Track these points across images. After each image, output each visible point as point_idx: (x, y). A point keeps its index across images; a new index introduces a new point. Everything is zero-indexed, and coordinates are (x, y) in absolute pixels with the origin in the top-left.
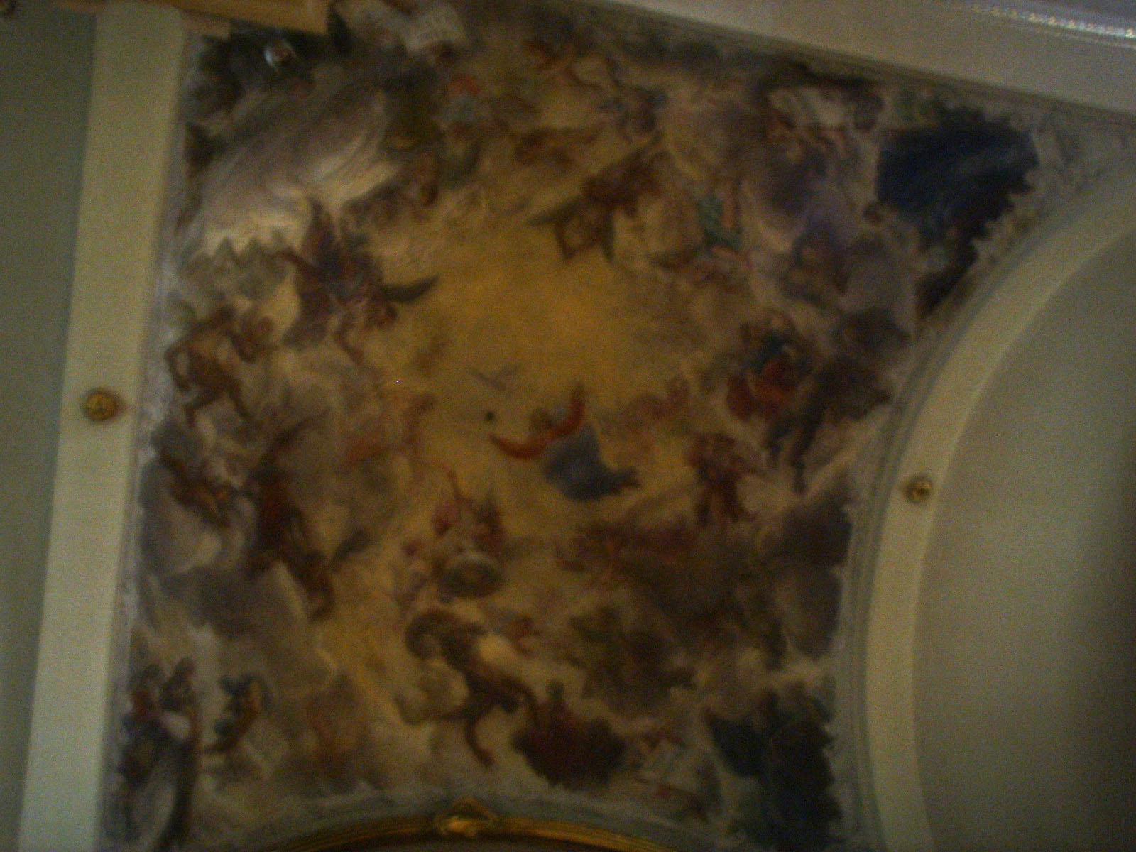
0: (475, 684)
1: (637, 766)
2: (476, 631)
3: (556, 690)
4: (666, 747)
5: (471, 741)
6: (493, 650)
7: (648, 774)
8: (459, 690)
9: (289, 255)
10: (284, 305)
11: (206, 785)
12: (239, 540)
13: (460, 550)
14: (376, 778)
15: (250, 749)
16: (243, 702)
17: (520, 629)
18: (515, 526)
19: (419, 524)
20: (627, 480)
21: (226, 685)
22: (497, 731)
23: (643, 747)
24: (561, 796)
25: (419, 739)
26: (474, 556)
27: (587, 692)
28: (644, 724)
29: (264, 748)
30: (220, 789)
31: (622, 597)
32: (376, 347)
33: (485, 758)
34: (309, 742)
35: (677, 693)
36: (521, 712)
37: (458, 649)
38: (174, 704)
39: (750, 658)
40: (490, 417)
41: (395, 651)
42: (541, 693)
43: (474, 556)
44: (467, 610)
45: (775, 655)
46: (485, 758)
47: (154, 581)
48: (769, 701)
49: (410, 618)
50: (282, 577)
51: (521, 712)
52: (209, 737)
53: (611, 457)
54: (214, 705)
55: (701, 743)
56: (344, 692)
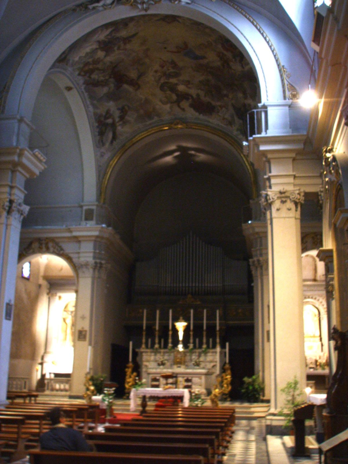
0: (177, 95)
1: (218, 112)
2: (177, 84)
3: (198, 95)
4: (224, 109)
5: (179, 106)
6: (181, 88)
7: (220, 114)
8: (174, 97)
9: (96, 49)
10: (101, 54)
11: (119, 128)
12: (112, 85)
13: (168, 70)
14: (159, 115)
15: (127, 118)
16: (123, 111)
17: (187, 83)
18: (181, 64)
19: (157, 67)
20: (203, 58)
21: (119, 109)
22: (185, 104)
23: (219, 108)
24: (201, 116)
25: (167, 107)
26: (172, 70)
27: (205, 96)
28: (219, 104)
29: (131, 117)
30: (122, 128)
31: (210, 78)
32: (128, 46)
33: (183, 110)
34: (142, 112)
35: (225, 98)
36: (190, 100)
37: (173, 89)
38: (106, 118)
39: (240, 95)
40: (165, 48)
41: (158, 91)
42: (195, 96)
43: (172, 70)
44: (174, 81)
45: (246, 98)
46: (183, 110)
47: (95, 102)
49: (160, 84)
50: (125, 86)
51: (190, 100)
52: (117, 120)
53: (198, 53)
54: (117, 114)
55: (232, 110)
56: (147, 101)
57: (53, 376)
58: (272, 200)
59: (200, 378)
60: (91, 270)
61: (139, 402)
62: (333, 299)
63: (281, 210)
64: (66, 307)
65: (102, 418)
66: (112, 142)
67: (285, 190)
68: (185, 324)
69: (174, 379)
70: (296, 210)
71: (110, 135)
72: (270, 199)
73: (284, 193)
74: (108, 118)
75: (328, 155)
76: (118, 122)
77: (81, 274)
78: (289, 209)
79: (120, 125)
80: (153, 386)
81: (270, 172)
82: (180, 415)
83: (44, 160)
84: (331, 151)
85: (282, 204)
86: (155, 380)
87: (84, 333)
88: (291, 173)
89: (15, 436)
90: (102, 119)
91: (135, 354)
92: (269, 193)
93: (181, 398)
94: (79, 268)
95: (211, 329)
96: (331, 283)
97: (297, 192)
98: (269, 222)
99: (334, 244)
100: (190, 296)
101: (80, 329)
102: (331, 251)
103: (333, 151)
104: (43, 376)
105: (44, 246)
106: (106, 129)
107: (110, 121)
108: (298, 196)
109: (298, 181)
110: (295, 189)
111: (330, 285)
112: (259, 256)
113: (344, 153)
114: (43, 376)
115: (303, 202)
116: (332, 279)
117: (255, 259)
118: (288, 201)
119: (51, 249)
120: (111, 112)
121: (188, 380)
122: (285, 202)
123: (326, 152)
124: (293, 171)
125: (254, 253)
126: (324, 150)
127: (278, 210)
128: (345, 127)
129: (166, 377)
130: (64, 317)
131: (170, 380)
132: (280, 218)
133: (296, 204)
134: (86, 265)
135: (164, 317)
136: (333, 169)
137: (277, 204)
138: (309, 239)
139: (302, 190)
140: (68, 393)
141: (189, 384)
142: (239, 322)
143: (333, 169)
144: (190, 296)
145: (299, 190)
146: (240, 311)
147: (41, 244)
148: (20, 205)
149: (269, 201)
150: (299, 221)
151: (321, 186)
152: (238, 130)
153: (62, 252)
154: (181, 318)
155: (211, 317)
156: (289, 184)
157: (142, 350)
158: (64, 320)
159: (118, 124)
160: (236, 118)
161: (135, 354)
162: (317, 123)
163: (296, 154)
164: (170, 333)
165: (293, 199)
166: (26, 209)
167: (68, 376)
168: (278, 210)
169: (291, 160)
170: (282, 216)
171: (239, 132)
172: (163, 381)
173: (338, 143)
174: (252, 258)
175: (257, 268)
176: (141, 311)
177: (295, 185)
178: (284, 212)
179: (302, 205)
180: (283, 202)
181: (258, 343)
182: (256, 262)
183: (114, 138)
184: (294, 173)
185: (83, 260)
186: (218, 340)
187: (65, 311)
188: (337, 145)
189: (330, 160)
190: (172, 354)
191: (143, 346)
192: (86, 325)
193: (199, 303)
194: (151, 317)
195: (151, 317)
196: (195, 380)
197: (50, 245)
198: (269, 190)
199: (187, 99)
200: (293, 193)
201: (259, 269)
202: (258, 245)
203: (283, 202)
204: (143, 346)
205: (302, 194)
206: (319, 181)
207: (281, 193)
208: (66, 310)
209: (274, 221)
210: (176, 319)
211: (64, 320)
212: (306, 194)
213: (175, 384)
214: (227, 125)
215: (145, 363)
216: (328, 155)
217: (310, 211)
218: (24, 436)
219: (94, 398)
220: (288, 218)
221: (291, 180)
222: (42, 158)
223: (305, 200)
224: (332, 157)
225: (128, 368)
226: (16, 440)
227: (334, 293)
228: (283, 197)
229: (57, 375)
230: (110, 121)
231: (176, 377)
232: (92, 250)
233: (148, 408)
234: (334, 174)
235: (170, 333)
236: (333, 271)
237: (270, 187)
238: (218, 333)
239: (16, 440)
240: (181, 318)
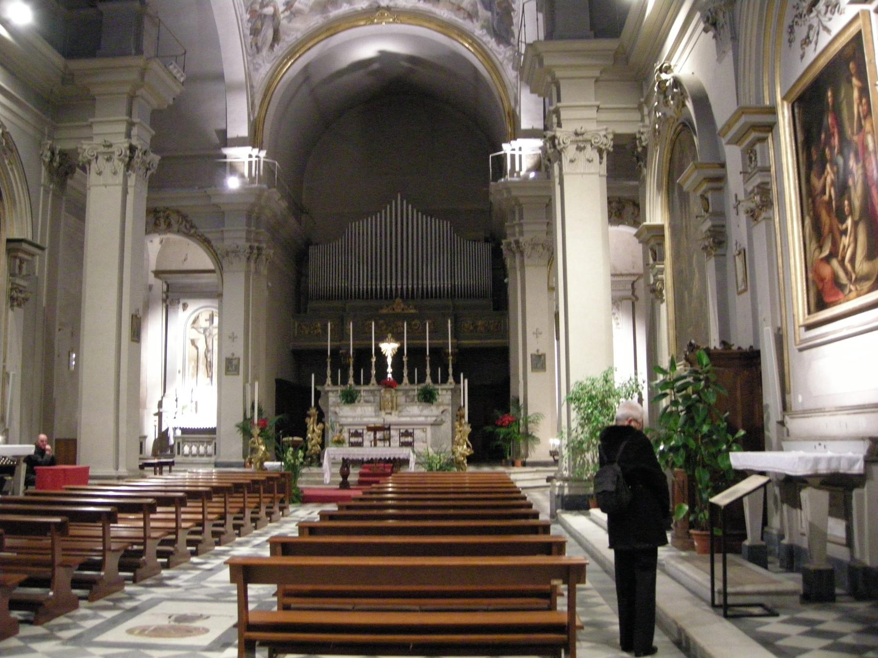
52: (281, 8)
57: (179, 433)
58: (562, 145)
59: (424, 431)
61: (337, 470)
62: (662, 301)
63: (576, 162)
66: (272, 46)
68: (395, 345)
70: (601, 163)
72: (559, 144)
73: (582, 134)
75: (664, 76)
76: (283, 12)
78: (590, 161)
79: (286, 17)
80: (353, 445)
81: (559, 100)
82: (390, 490)
83: (182, 79)
84: (668, 70)
86: (357, 434)
87: (235, 362)
88: (594, 103)
90: (257, 7)
91: (318, 394)
92: (558, 134)
94: (223, 257)
95: (438, 353)
96: (660, 276)
97: (604, 133)
99: (666, 216)
100: (398, 300)
101: (229, 356)
102: (661, 228)
103: (672, 71)
104: (163, 436)
105: (162, 220)
106: (262, 25)
107: (269, 10)
108: (604, 140)
109: (604, 116)
110: (600, 128)
111: (658, 280)
112: (517, 235)
114: (163, 436)
115: (611, 149)
116: (662, 271)
117: (511, 239)
119: (175, 227)
121: (407, 434)
122: (584, 148)
123: (661, 70)
125: (508, 232)
126: (658, 67)
127: (572, 161)
129: (374, 429)
130: (192, 337)
131: (379, 435)
132: (577, 174)
133: (600, 151)
134: (236, 252)
135: (362, 333)
136: (673, 99)
137: (570, 152)
138: (623, 208)
139: (610, 131)
140: (213, 459)
141: (409, 439)
142: (479, 342)
143: (673, 99)
144: (398, 300)
145: (606, 129)
146: (480, 323)
147: (158, 218)
148: (145, 153)
149: (558, 148)
150: (605, 179)
151: (641, 124)
152: (483, 27)
153: (193, 231)
154: (390, 335)
155: (438, 331)
157: (327, 388)
158: (193, 342)
159: (282, 16)
161: (318, 394)
163: (601, 73)
164: (374, 360)
165: (596, 145)
166: (155, 158)
167: (212, 431)
168: (572, 161)
170: (578, 171)
171: (485, 31)
172: (369, 436)
173: (680, 57)
174: (505, 238)
175: (514, 253)
176: (400, 323)
177: (599, 122)
179: (608, 153)
180: (580, 149)
182: (513, 245)
183: (276, 38)
184: (598, 103)
185: (228, 244)
186: (450, 371)
187: (193, 327)
190: (440, 392)
191: (329, 381)
193: (413, 311)
194: (340, 334)
195: (340, 334)
196: (418, 433)
197: (174, 218)
198: (558, 129)
201: (518, 256)
202: (517, 217)
203: (580, 149)
204: (329, 381)
205: (611, 137)
206: (637, 116)
207: (576, 134)
208: (195, 326)
209: (566, 179)
210: (381, 338)
211: (193, 342)
212: (617, 137)
214: (464, 19)
215: (332, 409)
217: (624, 162)
218: (184, 525)
219: (267, 464)
221: (593, 113)
222: (178, 75)
223: (614, 146)
224: (672, 80)
225: (310, 416)
227: (664, 292)
229: (185, 431)
230: (269, 10)
231: (389, 429)
233: (349, 479)
234: (673, 107)
236: (662, 259)
237: (559, 125)
240: (390, 335)
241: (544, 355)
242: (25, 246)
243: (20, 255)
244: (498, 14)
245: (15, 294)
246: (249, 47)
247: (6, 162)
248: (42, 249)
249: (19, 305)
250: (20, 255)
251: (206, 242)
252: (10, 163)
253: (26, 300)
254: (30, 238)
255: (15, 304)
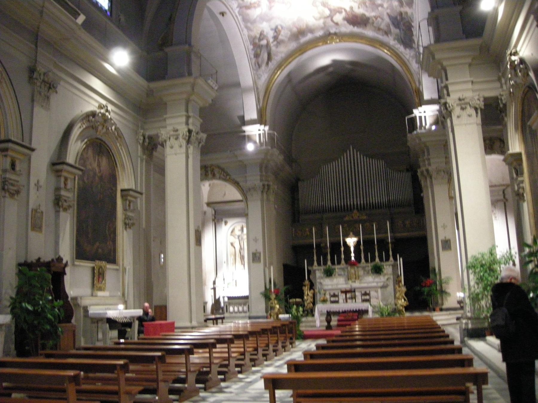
3: (352, 8)
27: (359, 8)
38: (260, 39)
48: (401, 14)
60: (260, 193)
61: (324, 318)
64: (232, 232)
65: (7, 382)
66: (267, 64)
67: (464, 97)
69: (353, 294)
70: (477, 116)
71: (266, 56)
73: (463, 99)
74: (263, 39)
75: (513, 58)
76: (272, 42)
77: (249, 197)
78: (470, 116)
81: (447, 79)
83: (216, 88)
84: (516, 54)
85: (462, 111)
86: (334, 296)
87: (258, 255)
89: (227, 355)
90: (257, 41)
93: (366, 312)
94: (247, 192)
95: (382, 243)
98: (450, 130)
99: (523, 146)
100: (355, 211)
102: (520, 154)
107: (264, 42)
108: (478, 102)
109: (477, 87)
113: (532, 54)
115: (483, 107)
116: (522, 182)
117: (423, 169)
118: (468, 107)
119: (218, 175)
120: (265, 33)
121: (366, 294)
124: (470, 77)
125: (421, 164)
127: (458, 117)
128: (537, 28)
129: (346, 292)
131: (349, 295)
133: (476, 109)
134: (254, 188)
135: (334, 233)
137: (457, 111)
138: (494, 143)
139: (481, 95)
140: (248, 314)
150: (480, 127)
155: (381, 229)
156: (467, 90)
158: (232, 244)
160: (392, 27)
161: (309, 272)
162: (495, 26)
163: (472, 60)
164: (342, 249)
166: (204, 136)
167: (246, 298)
168: (458, 117)
169: (467, 66)
171: (396, 42)
172: (342, 297)
175: (426, 178)
177: (474, 91)
178: (464, 119)
180: (463, 109)
181: (433, 254)
182: (425, 173)
184: (472, 79)
185: (249, 184)
187: (231, 235)
188: (522, 47)
189: (516, 63)
192: (259, 248)
194: (321, 234)
195: (321, 234)
196: (373, 293)
197: (216, 171)
199: (340, 12)
200: (472, 99)
201: (428, 179)
205: (482, 99)
207: (460, 100)
210: (346, 235)
211: (232, 244)
212: (486, 99)
213: (354, 298)
215: (318, 280)
216: (513, 58)
217: (492, 115)
219: (281, 316)
220: (470, 124)
221: (470, 86)
222: (214, 86)
223: (485, 105)
224: (519, 60)
225: (305, 286)
226: (228, 359)
228: (463, 104)
229: (229, 298)
230: (264, 42)
231: (354, 291)
232: (259, 173)
235: (342, 249)
237: (448, 95)
238: (390, 245)
239: (228, 359)
240: (351, 234)
241: (450, 240)
242: (131, 193)
243: (129, 198)
244: (403, 30)
245: (127, 221)
246: (253, 64)
247: (118, 145)
248: (141, 194)
249: (130, 228)
250: (129, 198)
251: (236, 184)
252: (120, 145)
253: (133, 224)
254: (134, 188)
255: (128, 226)
